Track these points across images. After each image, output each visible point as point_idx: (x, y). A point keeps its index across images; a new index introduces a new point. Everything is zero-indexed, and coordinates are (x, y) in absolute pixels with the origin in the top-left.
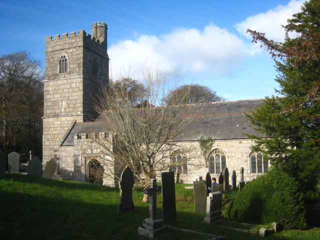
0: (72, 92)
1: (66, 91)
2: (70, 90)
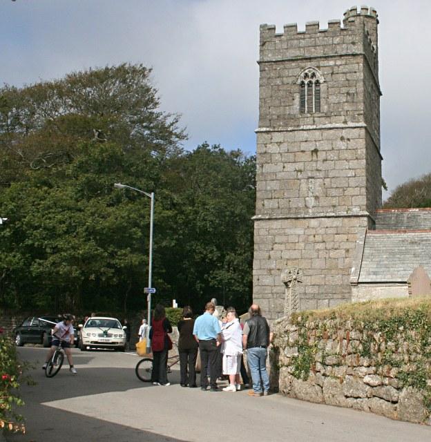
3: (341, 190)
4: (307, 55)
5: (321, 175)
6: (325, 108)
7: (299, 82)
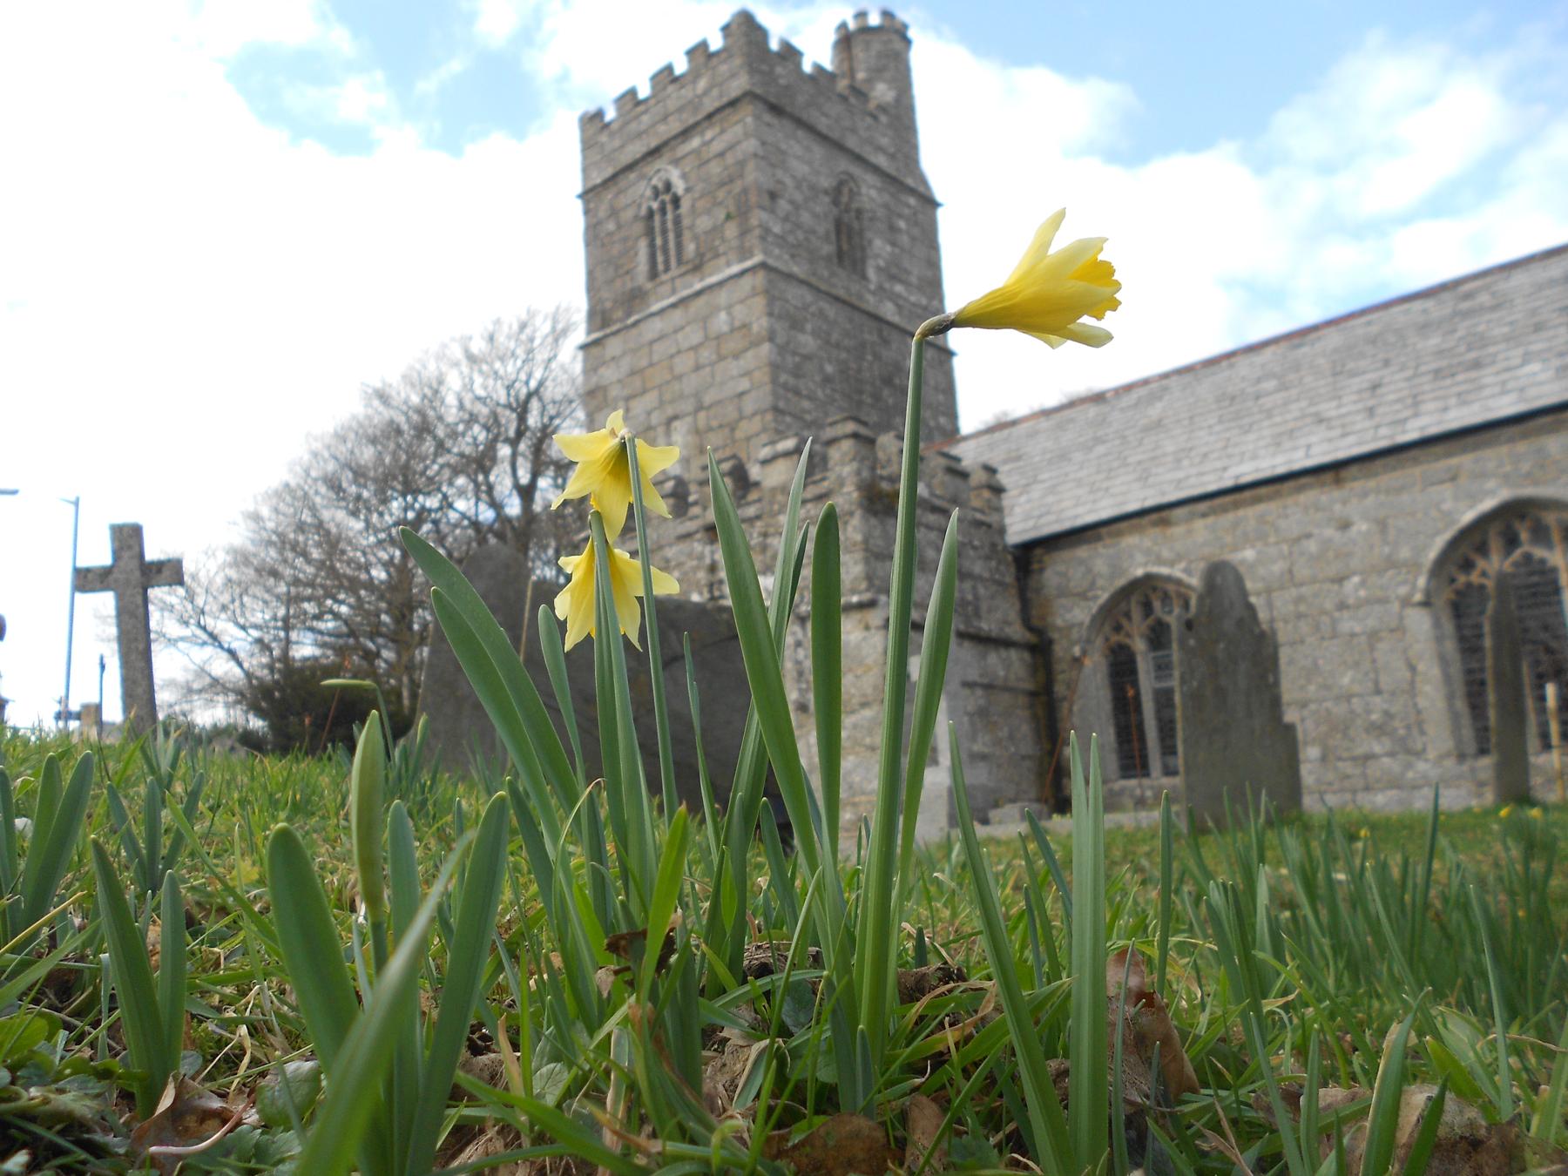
0: (712, 364)
1: (684, 363)
2: (706, 354)
3: (727, 430)
4: (654, 143)
5: (688, 406)
6: (690, 248)
7: (643, 211)
